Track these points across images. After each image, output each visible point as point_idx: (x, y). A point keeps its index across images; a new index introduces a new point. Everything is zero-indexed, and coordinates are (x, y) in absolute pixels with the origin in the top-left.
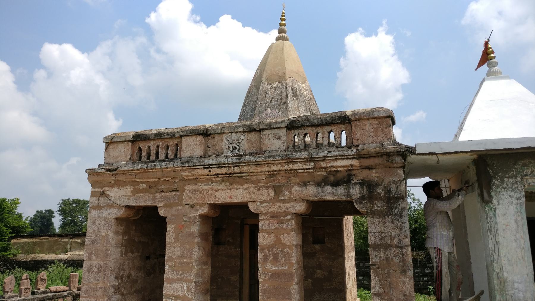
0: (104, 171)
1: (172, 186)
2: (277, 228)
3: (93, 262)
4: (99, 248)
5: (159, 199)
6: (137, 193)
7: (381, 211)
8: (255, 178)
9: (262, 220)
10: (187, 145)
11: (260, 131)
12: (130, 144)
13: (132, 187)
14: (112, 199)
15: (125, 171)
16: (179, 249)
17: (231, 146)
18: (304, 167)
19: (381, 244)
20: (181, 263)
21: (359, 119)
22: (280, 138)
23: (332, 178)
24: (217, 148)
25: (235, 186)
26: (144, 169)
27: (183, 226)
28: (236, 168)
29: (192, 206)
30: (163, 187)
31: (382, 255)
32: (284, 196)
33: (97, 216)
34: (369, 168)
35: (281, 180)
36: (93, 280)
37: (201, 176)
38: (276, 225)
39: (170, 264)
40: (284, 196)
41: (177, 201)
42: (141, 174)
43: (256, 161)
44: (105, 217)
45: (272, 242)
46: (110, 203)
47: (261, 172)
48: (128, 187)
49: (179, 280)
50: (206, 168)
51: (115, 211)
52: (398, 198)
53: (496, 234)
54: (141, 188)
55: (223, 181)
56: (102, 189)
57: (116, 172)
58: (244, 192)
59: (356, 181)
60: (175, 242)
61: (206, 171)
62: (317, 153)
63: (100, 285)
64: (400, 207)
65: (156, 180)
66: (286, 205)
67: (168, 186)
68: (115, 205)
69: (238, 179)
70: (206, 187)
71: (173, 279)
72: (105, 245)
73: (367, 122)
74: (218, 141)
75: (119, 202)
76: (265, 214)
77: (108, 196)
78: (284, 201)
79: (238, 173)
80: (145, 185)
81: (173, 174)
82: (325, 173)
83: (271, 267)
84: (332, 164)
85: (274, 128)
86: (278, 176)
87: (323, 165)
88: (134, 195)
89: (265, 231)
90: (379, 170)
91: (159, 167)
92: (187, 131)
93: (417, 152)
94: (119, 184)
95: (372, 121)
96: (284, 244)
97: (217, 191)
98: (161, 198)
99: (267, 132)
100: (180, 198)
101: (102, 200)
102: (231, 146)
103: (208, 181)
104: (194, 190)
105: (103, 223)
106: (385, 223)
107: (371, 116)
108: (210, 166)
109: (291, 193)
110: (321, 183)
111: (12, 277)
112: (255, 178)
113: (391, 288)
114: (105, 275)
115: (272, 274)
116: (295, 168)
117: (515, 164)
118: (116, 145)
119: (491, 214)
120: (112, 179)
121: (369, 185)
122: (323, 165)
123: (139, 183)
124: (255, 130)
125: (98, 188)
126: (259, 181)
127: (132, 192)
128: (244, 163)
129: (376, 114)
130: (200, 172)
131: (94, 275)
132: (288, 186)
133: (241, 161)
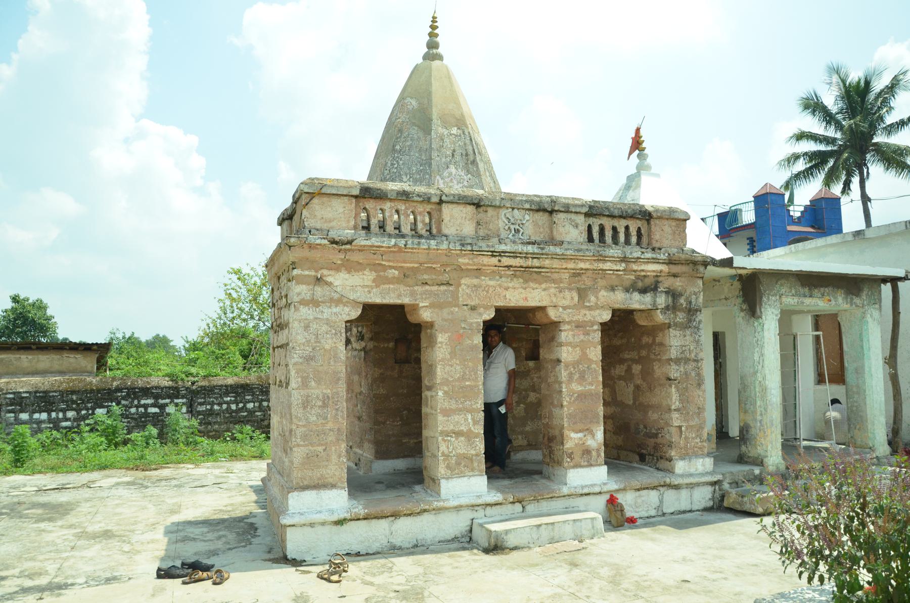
0: (326, 242)
1: (441, 277)
2: (582, 341)
3: (313, 391)
4: (321, 369)
5: (421, 294)
6: (384, 284)
7: (682, 324)
8: (556, 276)
9: (565, 330)
10: (452, 216)
11: (551, 212)
12: (354, 200)
13: (374, 274)
14: (339, 289)
15: (364, 246)
16: (458, 368)
17: (512, 227)
18: (615, 268)
19: (682, 358)
20: (462, 388)
21: (659, 218)
22: (577, 226)
23: (640, 284)
24: (491, 227)
25: (532, 284)
26: (400, 248)
27: (461, 336)
28: (535, 260)
29: (473, 308)
30: (426, 277)
31: (682, 369)
32: (589, 301)
33: (312, 317)
34: (675, 276)
35: (587, 281)
36: (315, 418)
37: (485, 265)
38: (582, 337)
39: (446, 388)
40: (589, 301)
41: (450, 300)
42: (391, 255)
43: (563, 255)
44: (327, 319)
45: (577, 357)
46: (336, 296)
47: (566, 269)
48: (365, 272)
49: (460, 410)
50: (495, 256)
51: (347, 309)
52: (697, 310)
53: (762, 347)
54: (390, 276)
55: (515, 276)
56: (317, 271)
57: (348, 247)
58: (543, 293)
59: (662, 289)
60: (452, 358)
61: (494, 261)
62: (631, 253)
63: (330, 425)
64: (697, 320)
65: (416, 265)
66: (592, 312)
67: (434, 277)
68: (345, 300)
69: (535, 276)
70: (492, 283)
71: (451, 409)
72: (332, 363)
73: (666, 222)
74: (492, 216)
75: (352, 296)
76: (569, 323)
77: (329, 284)
78: (590, 308)
79: (537, 268)
80: (397, 272)
81: (444, 259)
82: (633, 277)
83: (576, 387)
84: (643, 267)
85: (571, 212)
86: (584, 277)
87: (635, 267)
88: (377, 286)
89: (569, 344)
90: (683, 279)
91: (426, 247)
92: (454, 195)
93: (734, 265)
94: (350, 267)
95: (670, 222)
96: (590, 360)
97: (507, 289)
98: (425, 292)
99: (562, 216)
100: (455, 296)
101: (319, 291)
102: (512, 227)
103: (494, 274)
104: (475, 286)
105: (325, 328)
106: (685, 336)
107: (672, 216)
108: (501, 254)
109: (597, 298)
110: (631, 288)
111: (440, 418)
112: (556, 276)
113: (688, 402)
114: (337, 410)
115: (578, 396)
116: (605, 268)
117: (776, 283)
118: (325, 199)
119: (759, 329)
120: (338, 258)
121: (673, 294)
122: (635, 267)
123: (385, 268)
124: (545, 210)
125: (309, 269)
126: (561, 281)
127: (374, 281)
128: (547, 254)
129: (676, 216)
130: (487, 260)
131: (316, 410)
132: (594, 289)
133: (544, 252)
